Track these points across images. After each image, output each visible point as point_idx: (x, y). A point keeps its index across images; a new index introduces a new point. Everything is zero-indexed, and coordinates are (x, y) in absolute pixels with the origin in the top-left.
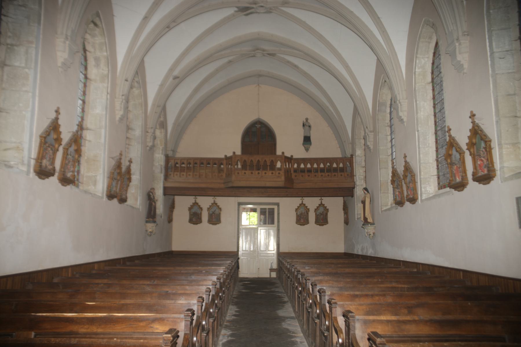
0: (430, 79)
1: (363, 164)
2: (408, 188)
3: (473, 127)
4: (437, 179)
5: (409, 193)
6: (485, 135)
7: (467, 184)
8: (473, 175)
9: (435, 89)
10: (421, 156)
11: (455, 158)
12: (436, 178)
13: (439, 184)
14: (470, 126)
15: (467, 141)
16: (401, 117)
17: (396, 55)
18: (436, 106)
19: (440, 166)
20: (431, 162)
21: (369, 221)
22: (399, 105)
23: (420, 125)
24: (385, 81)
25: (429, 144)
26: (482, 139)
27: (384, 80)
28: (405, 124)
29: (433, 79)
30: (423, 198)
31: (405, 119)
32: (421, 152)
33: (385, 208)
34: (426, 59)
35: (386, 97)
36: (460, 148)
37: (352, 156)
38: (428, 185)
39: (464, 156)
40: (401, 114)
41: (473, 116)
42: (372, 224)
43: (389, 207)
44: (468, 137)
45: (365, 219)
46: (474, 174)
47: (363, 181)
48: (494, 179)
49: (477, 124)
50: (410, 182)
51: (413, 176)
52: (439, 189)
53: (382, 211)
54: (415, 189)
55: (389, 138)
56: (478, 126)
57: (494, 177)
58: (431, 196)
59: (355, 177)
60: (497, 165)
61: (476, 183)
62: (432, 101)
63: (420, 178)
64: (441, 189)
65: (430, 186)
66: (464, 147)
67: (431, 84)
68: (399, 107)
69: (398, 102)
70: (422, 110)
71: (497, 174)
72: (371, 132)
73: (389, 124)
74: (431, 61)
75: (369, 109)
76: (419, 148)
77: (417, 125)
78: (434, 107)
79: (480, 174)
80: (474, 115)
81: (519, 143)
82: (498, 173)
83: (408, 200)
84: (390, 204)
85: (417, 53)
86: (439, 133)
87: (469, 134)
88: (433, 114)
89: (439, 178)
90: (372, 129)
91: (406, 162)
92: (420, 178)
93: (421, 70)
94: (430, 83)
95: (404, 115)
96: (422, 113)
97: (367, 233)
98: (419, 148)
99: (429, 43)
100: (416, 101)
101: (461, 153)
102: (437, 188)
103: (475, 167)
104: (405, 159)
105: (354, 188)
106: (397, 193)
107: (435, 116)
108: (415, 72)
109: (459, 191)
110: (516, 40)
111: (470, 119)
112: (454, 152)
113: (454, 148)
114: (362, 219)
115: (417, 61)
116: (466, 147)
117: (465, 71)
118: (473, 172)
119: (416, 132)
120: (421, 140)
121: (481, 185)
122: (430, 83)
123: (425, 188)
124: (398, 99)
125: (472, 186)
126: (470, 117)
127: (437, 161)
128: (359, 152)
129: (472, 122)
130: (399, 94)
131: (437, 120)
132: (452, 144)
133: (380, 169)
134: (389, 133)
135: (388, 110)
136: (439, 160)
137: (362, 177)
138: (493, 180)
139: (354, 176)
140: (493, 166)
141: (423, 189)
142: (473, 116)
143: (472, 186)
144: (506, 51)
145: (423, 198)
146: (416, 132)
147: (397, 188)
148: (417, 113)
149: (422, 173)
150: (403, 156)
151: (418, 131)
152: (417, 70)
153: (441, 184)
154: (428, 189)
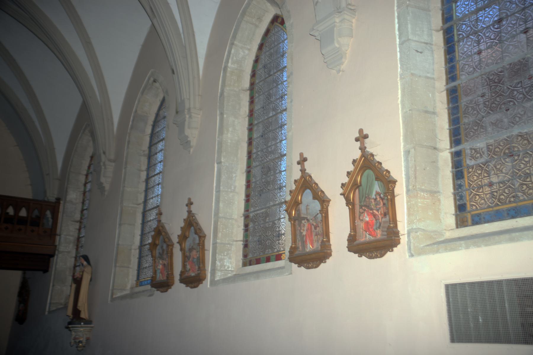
0: (246, 84)
1: (78, 216)
2: (185, 258)
3: (188, 217)
4: (242, 247)
5: (188, 267)
6: (200, 229)
7: (173, 284)
8: (181, 275)
9: (256, 100)
10: (221, 205)
11: (307, 209)
12: (241, 245)
13: (245, 256)
14: (185, 215)
15: (179, 233)
16: (187, 137)
17: (194, 35)
18: (255, 128)
19: (251, 225)
20: (236, 217)
21: (83, 315)
22: (103, 167)
23: (224, 154)
24: (155, 81)
25: (235, 187)
26: (165, 242)
27: (152, 79)
28: (192, 150)
29: (252, 84)
30: (217, 278)
31: (194, 143)
32: (221, 199)
33: (119, 295)
34: (247, 52)
35: (150, 107)
36: (170, 239)
37: (58, 200)
38: (226, 255)
39: (172, 250)
40: (103, 180)
41: (362, 137)
42: (88, 322)
43: (127, 292)
44: (181, 228)
45: (76, 312)
46: (182, 273)
47: (71, 245)
48: (172, 287)
49: (163, 223)
50: (191, 250)
51: (201, 236)
52: (244, 265)
53: (113, 299)
54: (201, 261)
55: (144, 175)
56: (163, 227)
57: (172, 285)
58: (229, 275)
59: (58, 238)
60: (403, 227)
61: (183, 285)
62: (247, 119)
63: (215, 244)
64: (250, 265)
65: (230, 258)
66: (175, 239)
67: (248, 92)
68: (187, 119)
69: (102, 164)
70: (230, 129)
71: (402, 241)
72: (110, 160)
73: (147, 152)
74: (253, 57)
75: (113, 124)
76: (218, 191)
77: (220, 152)
78: (250, 130)
79: (365, 237)
80: (192, 204)
81: (439, 192)
82: (404, 239)
83: (182, 281)
84: (129, 287)
85: (234, 37)
86: (256, 171)
87: (182, 224)
88: (246, 138)
89: (246, 246)
90: (112, 157)
91: (189, 212)
92: (215, 244)
93: (235, 66)
94: (246, 90)
95: (106, 181)
96: (229, 135)
97: (75, 339)
98: (218, 191)
99: (257, 26)
100: (222, 114)
101: (170, 245)
102: (241, 264)
103: (184, 266)
104: (190, 208)
105: (52, 256)
106: (160, 267)
107: (250, 143)
108: (226, 68)
109: (162, 292)
110: (438, 31)
111: (187, 208)
112: (307, 197)
113: (192, 228)
114: (70, 311)
115: (233, 51)
116: (177, 240)
117: (343, 67)
118: (350, 235)
119: (216, 165)
120: (223, 178)
121: (188, 288)
122: (246, 90)
123: (221, 260)
124: (187, 106)
125: (178, 287)
126: (187, 205)
127: (246, 217)
128: (74, 196)
129: (301, 170)
130: (189, 99)
131: (254, 151)
132: (160, 232)
133: (120, 225)
134: (144, 167)
135: (149, 130)
136: (251, 215)
137: (72, 238)
138: (171, 288)
139: (55, 235)
140: (396, 226)
141: (218, 263)
142: (362, 137)
143: (178, 287)
144: (425, 43)
145: (217, 278)
146: (216, 165)
147: (161, 257)
148: (221, 132)
149: (220, 235)
150: (186, 202)
151: (219, 163)
152: (230, 65)
153: (250, 256)
154: (227, 263)
